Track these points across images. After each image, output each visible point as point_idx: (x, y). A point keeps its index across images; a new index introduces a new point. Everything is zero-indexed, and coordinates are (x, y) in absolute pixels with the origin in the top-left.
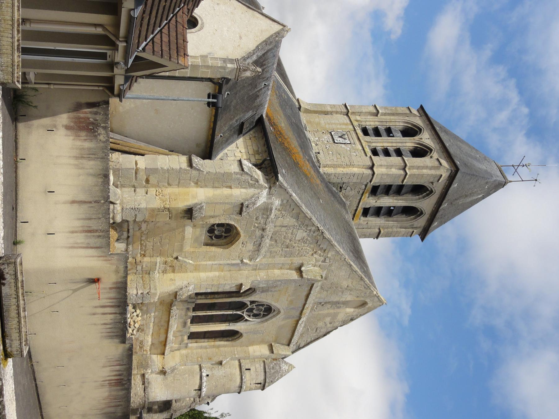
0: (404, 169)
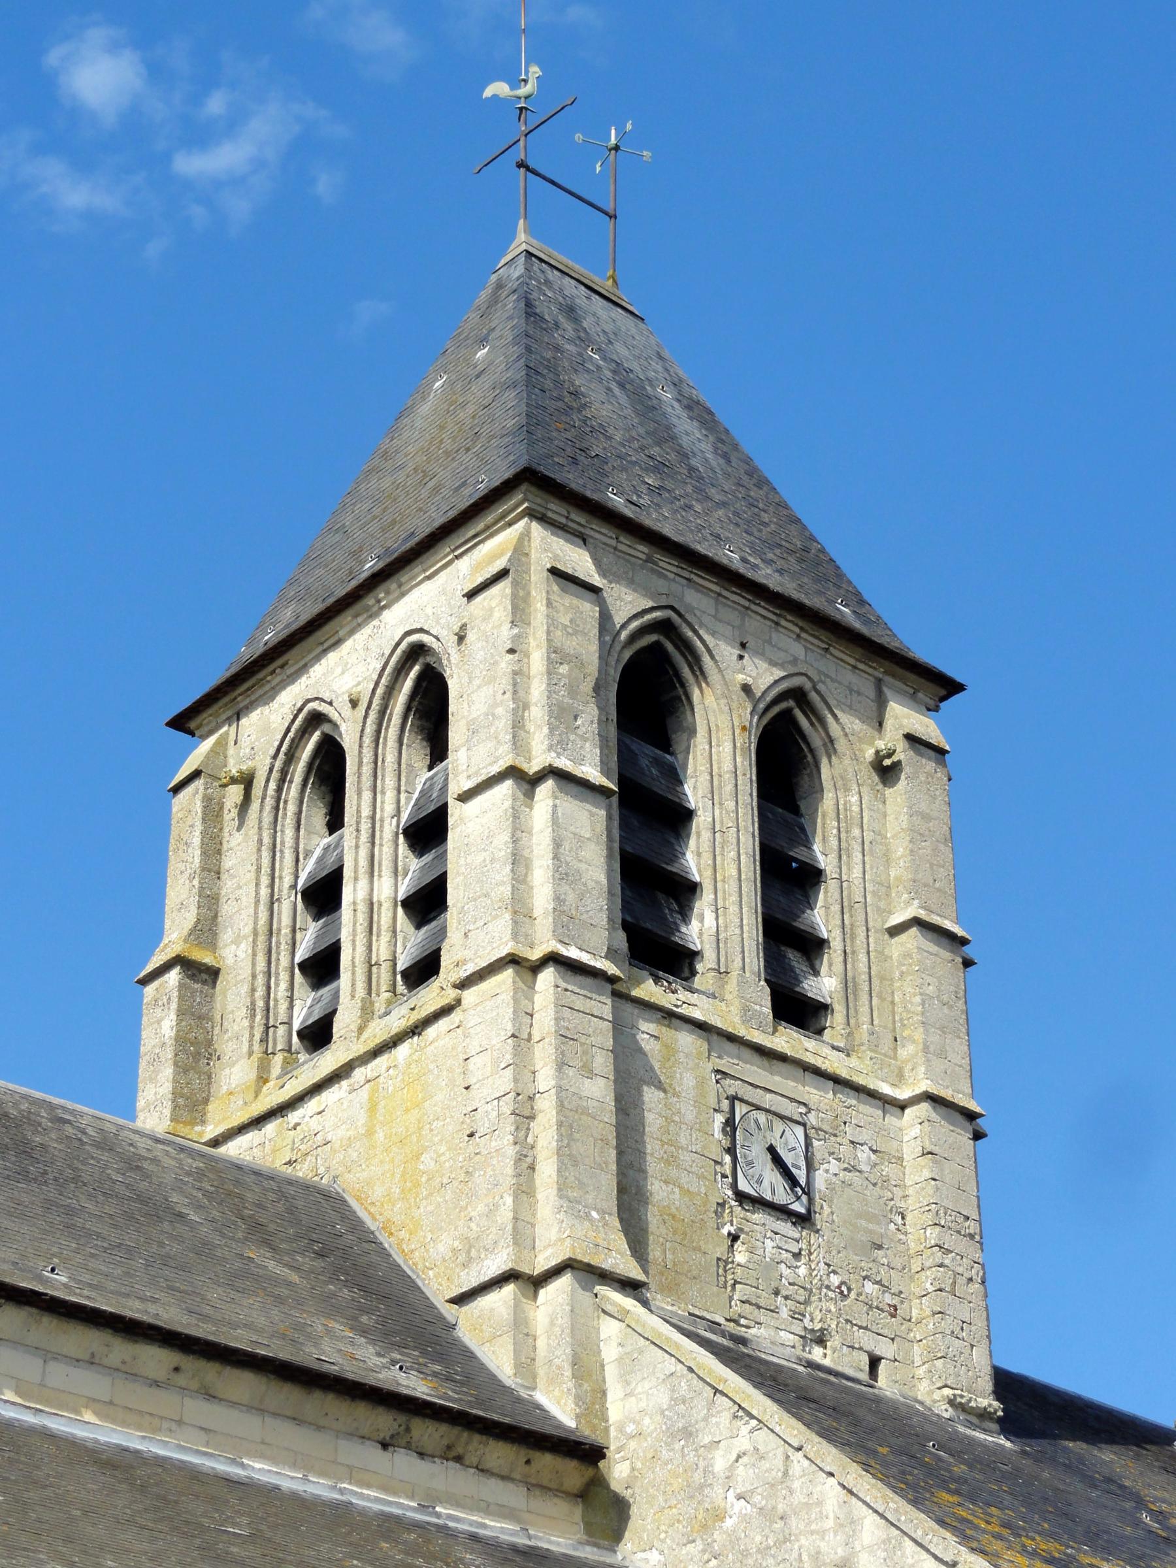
0: (536, 968)
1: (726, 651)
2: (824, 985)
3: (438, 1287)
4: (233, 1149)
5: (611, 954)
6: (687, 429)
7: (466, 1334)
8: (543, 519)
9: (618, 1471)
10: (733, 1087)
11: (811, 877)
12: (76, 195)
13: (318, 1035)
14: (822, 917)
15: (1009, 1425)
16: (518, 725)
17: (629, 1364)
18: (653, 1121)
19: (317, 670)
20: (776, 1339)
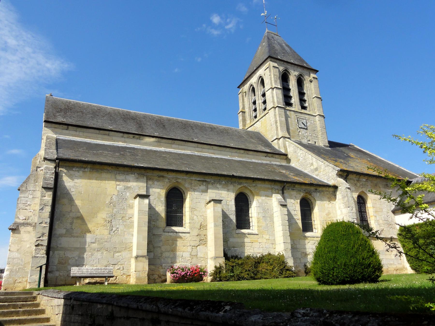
1: (292, 71)
2: (306, 105)
3: (270, 141)
4: (248, 130)
5: (283, 105)
6: (286, 48)
7: (273, 145)
8: (271, 61)
9: (289, 156)
10: (298, 117)
11: (304, 94)
12: (215, 33)
13: (256, 117)
14: (306, 98)
15: (330, 147)
16: (271, 83)
17: (289, 146)
18: (290, 121)
19: (251, 80)
20: (305, 141)
